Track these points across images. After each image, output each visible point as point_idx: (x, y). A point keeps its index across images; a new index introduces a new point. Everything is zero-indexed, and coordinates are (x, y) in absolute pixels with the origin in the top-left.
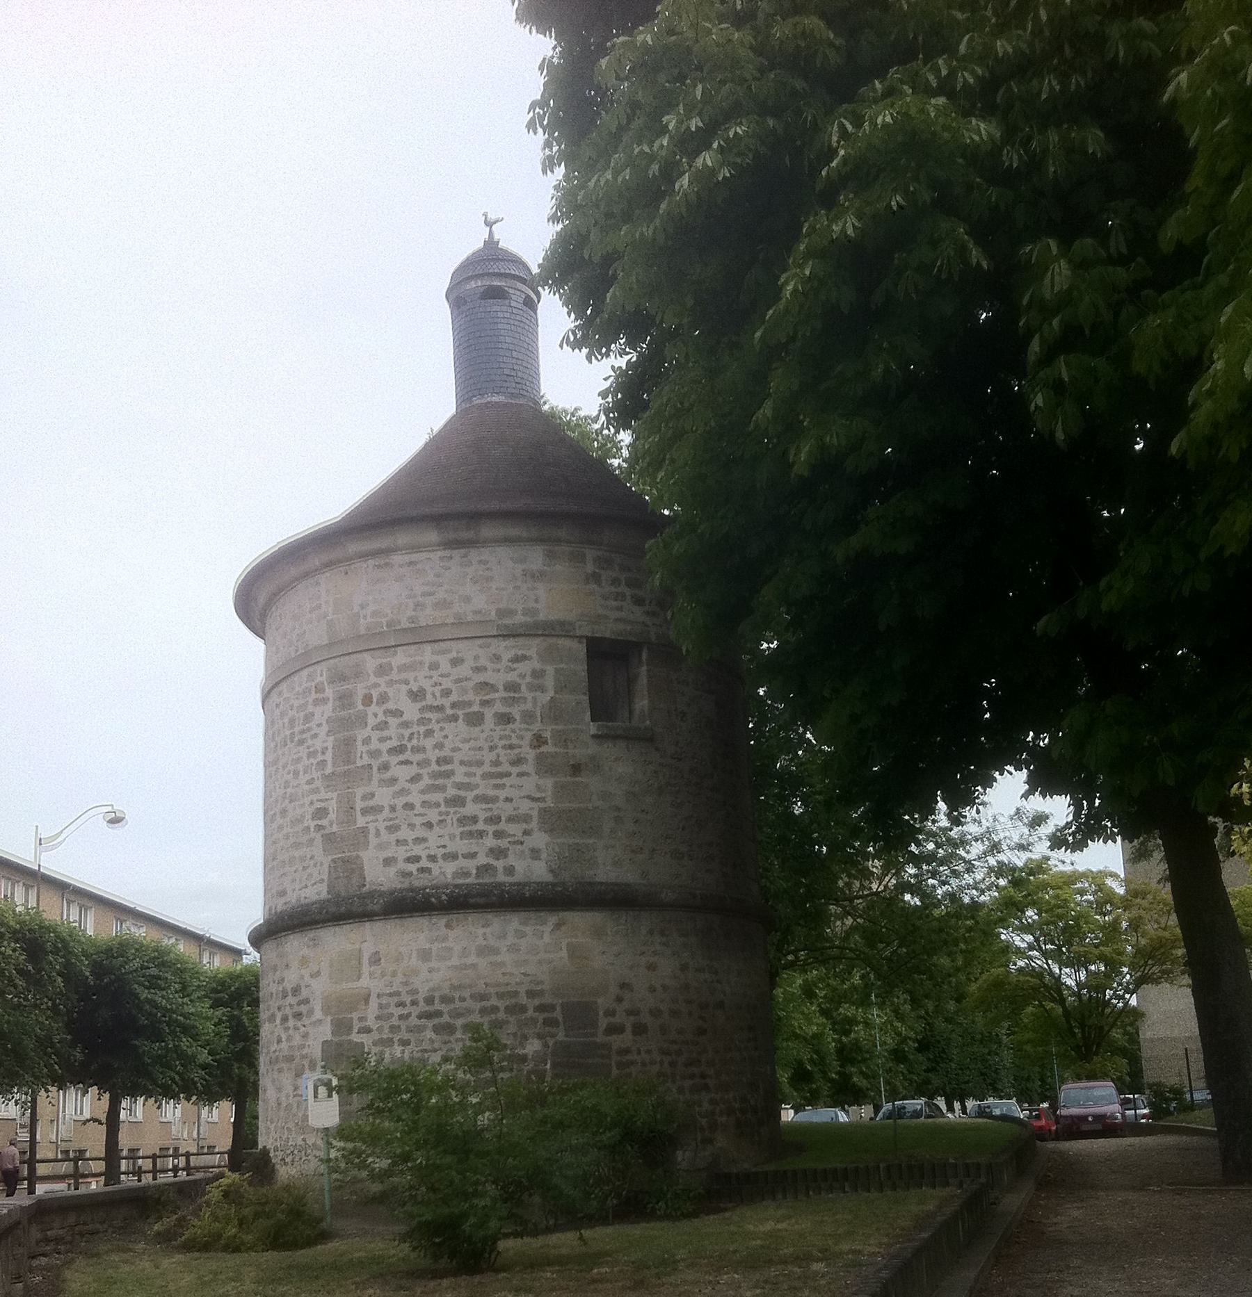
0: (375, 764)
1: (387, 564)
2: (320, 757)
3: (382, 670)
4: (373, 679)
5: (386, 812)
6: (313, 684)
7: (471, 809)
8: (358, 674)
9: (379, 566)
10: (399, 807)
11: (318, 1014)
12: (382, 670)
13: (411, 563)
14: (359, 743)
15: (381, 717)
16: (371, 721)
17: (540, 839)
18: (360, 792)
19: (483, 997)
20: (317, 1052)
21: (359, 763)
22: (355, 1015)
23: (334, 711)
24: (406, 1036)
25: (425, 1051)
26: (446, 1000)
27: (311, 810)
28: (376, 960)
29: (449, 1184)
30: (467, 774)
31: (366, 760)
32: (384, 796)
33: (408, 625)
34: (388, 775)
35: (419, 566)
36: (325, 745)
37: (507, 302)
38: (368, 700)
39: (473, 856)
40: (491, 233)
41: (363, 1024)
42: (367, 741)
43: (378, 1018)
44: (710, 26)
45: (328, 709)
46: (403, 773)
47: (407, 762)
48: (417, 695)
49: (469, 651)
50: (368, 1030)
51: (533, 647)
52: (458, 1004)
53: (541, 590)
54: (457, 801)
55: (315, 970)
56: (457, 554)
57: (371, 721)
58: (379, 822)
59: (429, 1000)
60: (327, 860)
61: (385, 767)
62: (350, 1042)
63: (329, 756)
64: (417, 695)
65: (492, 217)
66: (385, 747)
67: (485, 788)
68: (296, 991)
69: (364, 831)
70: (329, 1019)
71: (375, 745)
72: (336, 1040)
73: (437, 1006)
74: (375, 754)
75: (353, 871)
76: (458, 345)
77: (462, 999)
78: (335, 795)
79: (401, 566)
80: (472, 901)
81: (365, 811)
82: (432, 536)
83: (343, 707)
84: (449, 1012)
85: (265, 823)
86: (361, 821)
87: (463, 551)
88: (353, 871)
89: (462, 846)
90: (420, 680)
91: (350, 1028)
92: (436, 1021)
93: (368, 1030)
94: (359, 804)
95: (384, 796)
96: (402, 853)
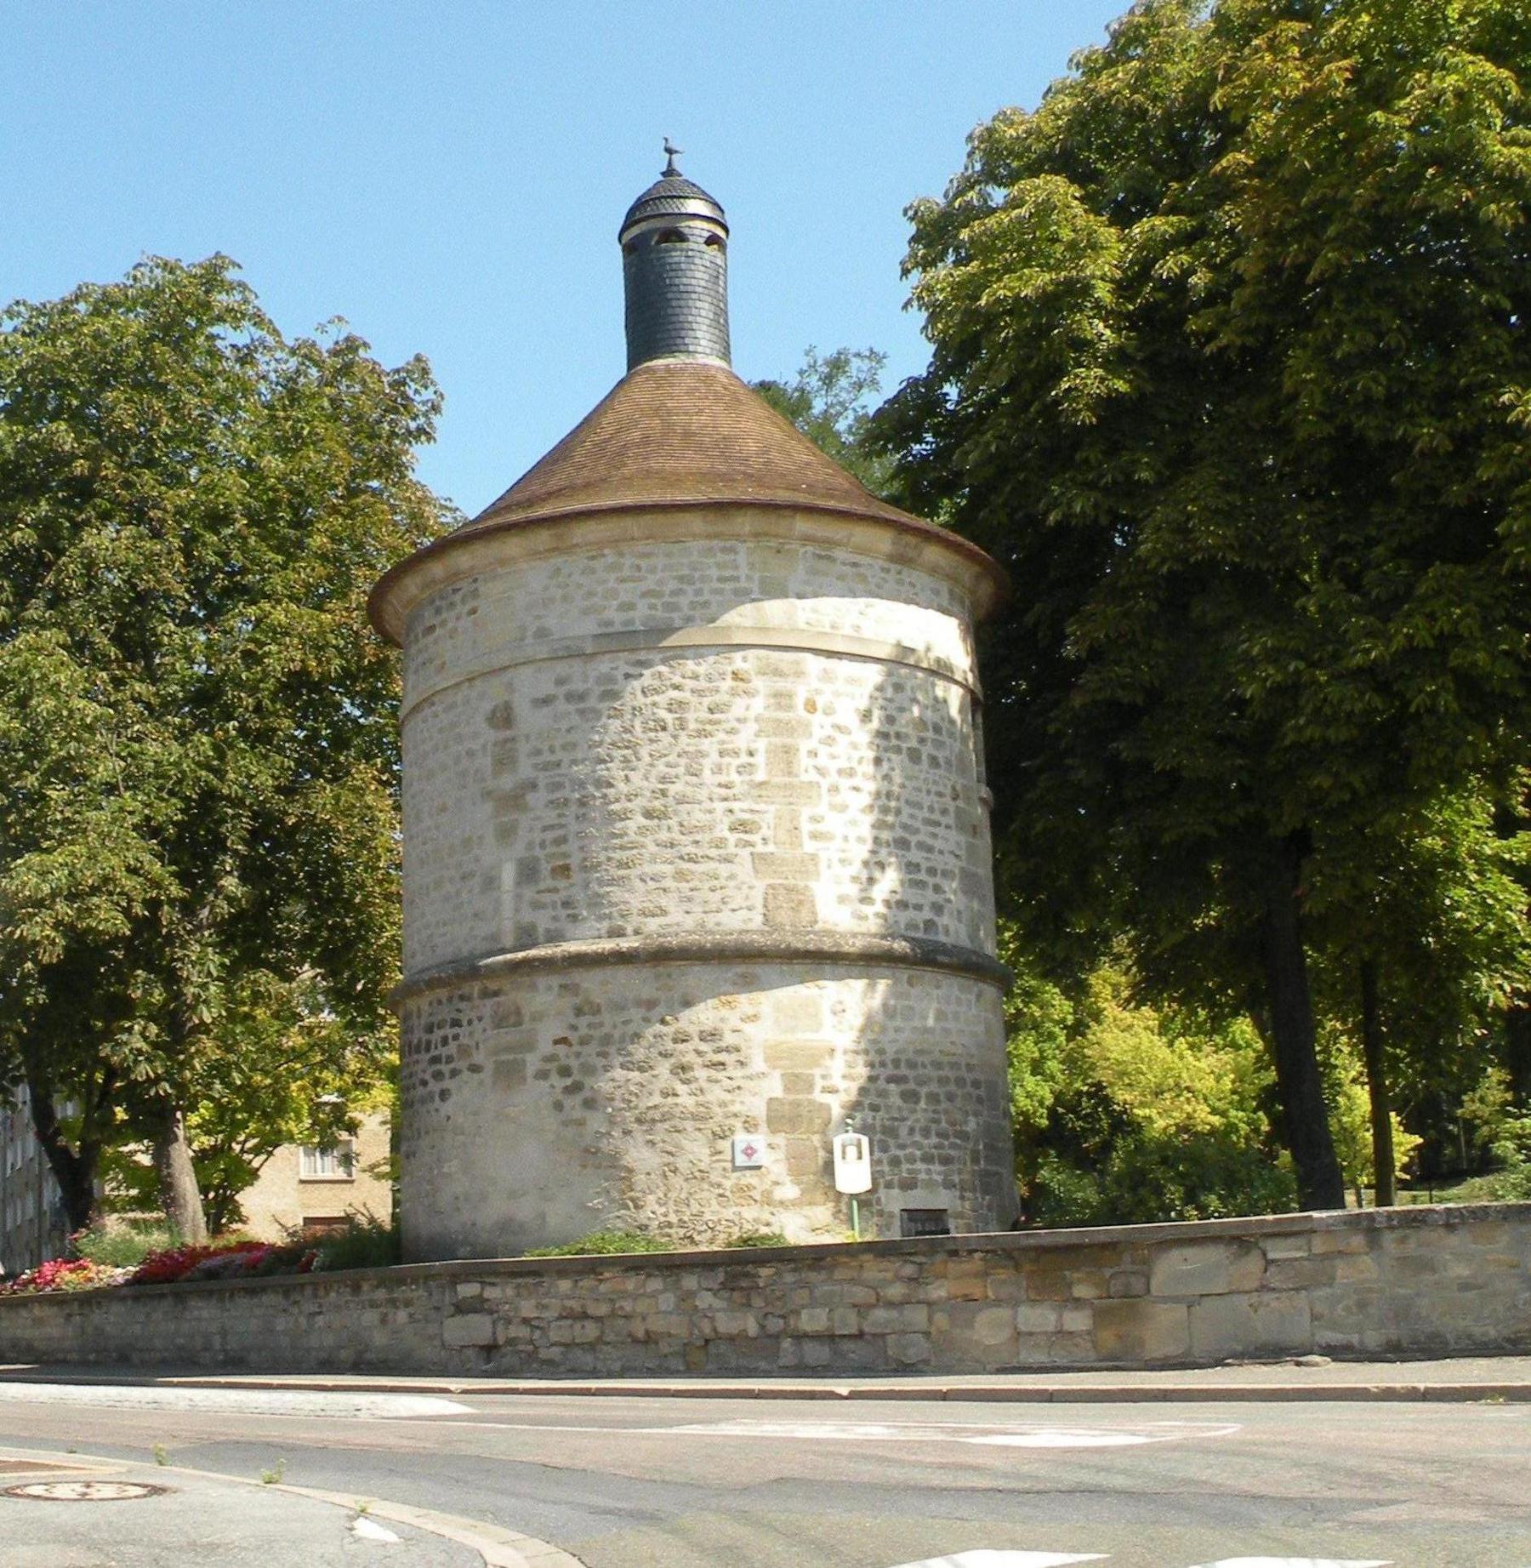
0: (825, 784)
1: (829, 558)
2: (744, 759)
3: (826, 676)
4: (816, 684)
5: (838, 842)
6: (730, 669)
9: (820, 557)
10: (852, 838)
13: (855, 565)
14: (803, 753)
15: (829, 731)
16: (818, 733)
19: (938, 1065)
21: (805, 778)
22: (817, 1072)
23: (767, 707)
24: (878, 1101)
25: (896, 1119)
26: (912, 1065)
27: (728, 821)
29: (640, 1334)
30: (912, 816)
31: (813, 776)
33: (851, 632)
34: (838, 799)
35: (862, 570)
36: (753, 746)
37: (684, 245)
39: (918, 907)
40: (670, 164)
41: (827, 1083)
42: (814, 754)
43: (844, 1077)
45: (758, 705)
47: (856, 789)
50: (833, 1091)
52: (921, 1071)
55: (751, 1012)
56: (894, 567)
57: (818, 733)
59: (896, 1063)
60: (760, 885)
61: (834, 789)
62: (811, 1102)
63: (760, 759)
65: (673, 145)
66: (833, 766)
69: (814, 858)
70: (777, 1074)
71: (822, 760)
72: (791, 1097)
73: (904, 1071)
74: (820, 771)
75: (801, 903)
76: (627, 279)
77: (924, 1066)
78: (772, 808)
79: (844, 564)
80: (941, 958)
81: (814, 836)
83: (779, 707)
84: (915, 1078)
86: (810, 846)
87: (899, 567)
88: (801, 903)
91: (810, 1087)
92: (903, 1087)
93: (833, 1091)
94: (806, 827)
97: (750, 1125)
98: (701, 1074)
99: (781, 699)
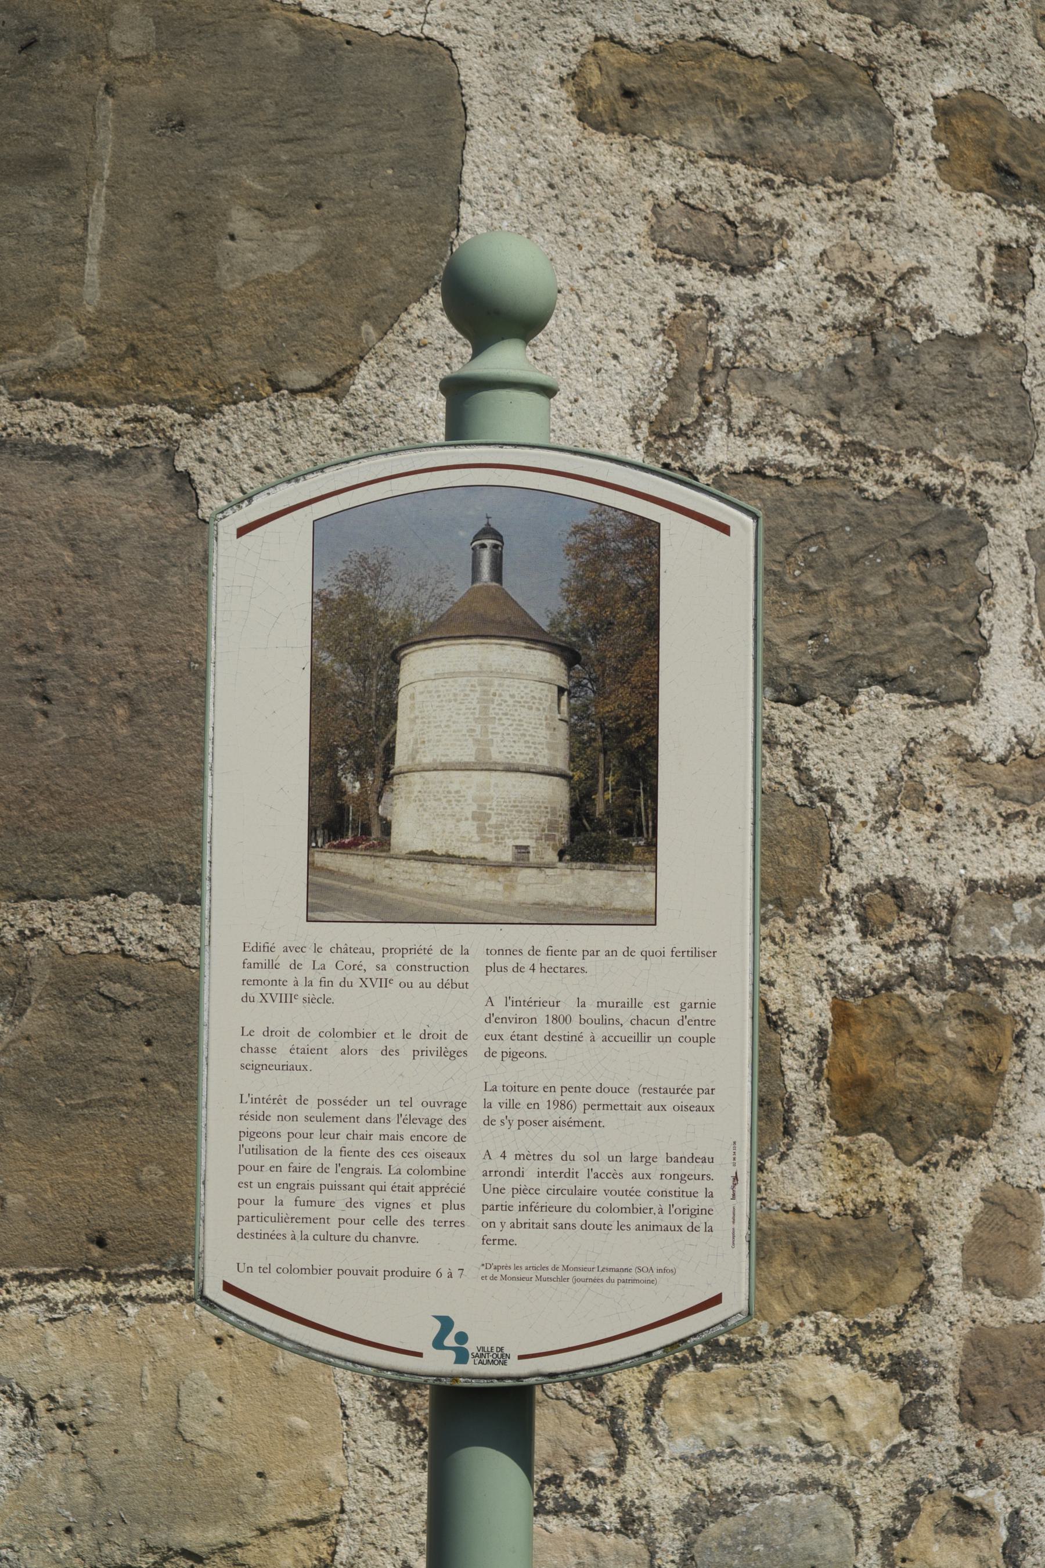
3: (500, 685)
7: (527, 738)
8: (491, 685)
11: (470, 801)
12: (500, 685)
17: (546, 751)
18: (490, 726)
20: (469, 815)
28: (496, 785)
32: (500, 729)
38: (494, 695)
44: (106, 174)
45: (477, 695)
46: (507, 723)
48: (512, 696)
49: (532, 685)
51: (546, 686)
53: (549, 668)
54: (524, 735)
58: (498, 738)
64: (512, 696)
67: (532, 732)
68: (457, 792)
82: (523, 644)
85: (202, 677)
89: (527, 751)
90: (513, 691)
95: (500, 729)
96: (505, 750)
97: (467, 819)
98: (454, 803)
99: (485, 693)
